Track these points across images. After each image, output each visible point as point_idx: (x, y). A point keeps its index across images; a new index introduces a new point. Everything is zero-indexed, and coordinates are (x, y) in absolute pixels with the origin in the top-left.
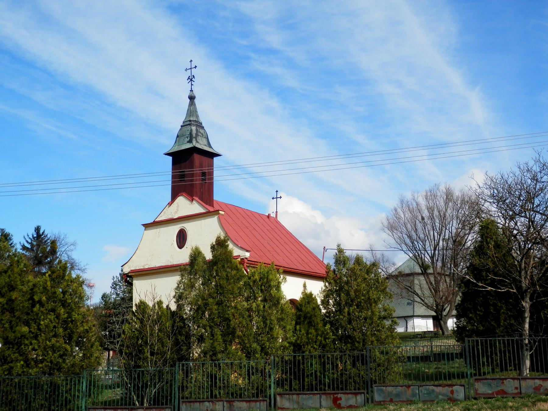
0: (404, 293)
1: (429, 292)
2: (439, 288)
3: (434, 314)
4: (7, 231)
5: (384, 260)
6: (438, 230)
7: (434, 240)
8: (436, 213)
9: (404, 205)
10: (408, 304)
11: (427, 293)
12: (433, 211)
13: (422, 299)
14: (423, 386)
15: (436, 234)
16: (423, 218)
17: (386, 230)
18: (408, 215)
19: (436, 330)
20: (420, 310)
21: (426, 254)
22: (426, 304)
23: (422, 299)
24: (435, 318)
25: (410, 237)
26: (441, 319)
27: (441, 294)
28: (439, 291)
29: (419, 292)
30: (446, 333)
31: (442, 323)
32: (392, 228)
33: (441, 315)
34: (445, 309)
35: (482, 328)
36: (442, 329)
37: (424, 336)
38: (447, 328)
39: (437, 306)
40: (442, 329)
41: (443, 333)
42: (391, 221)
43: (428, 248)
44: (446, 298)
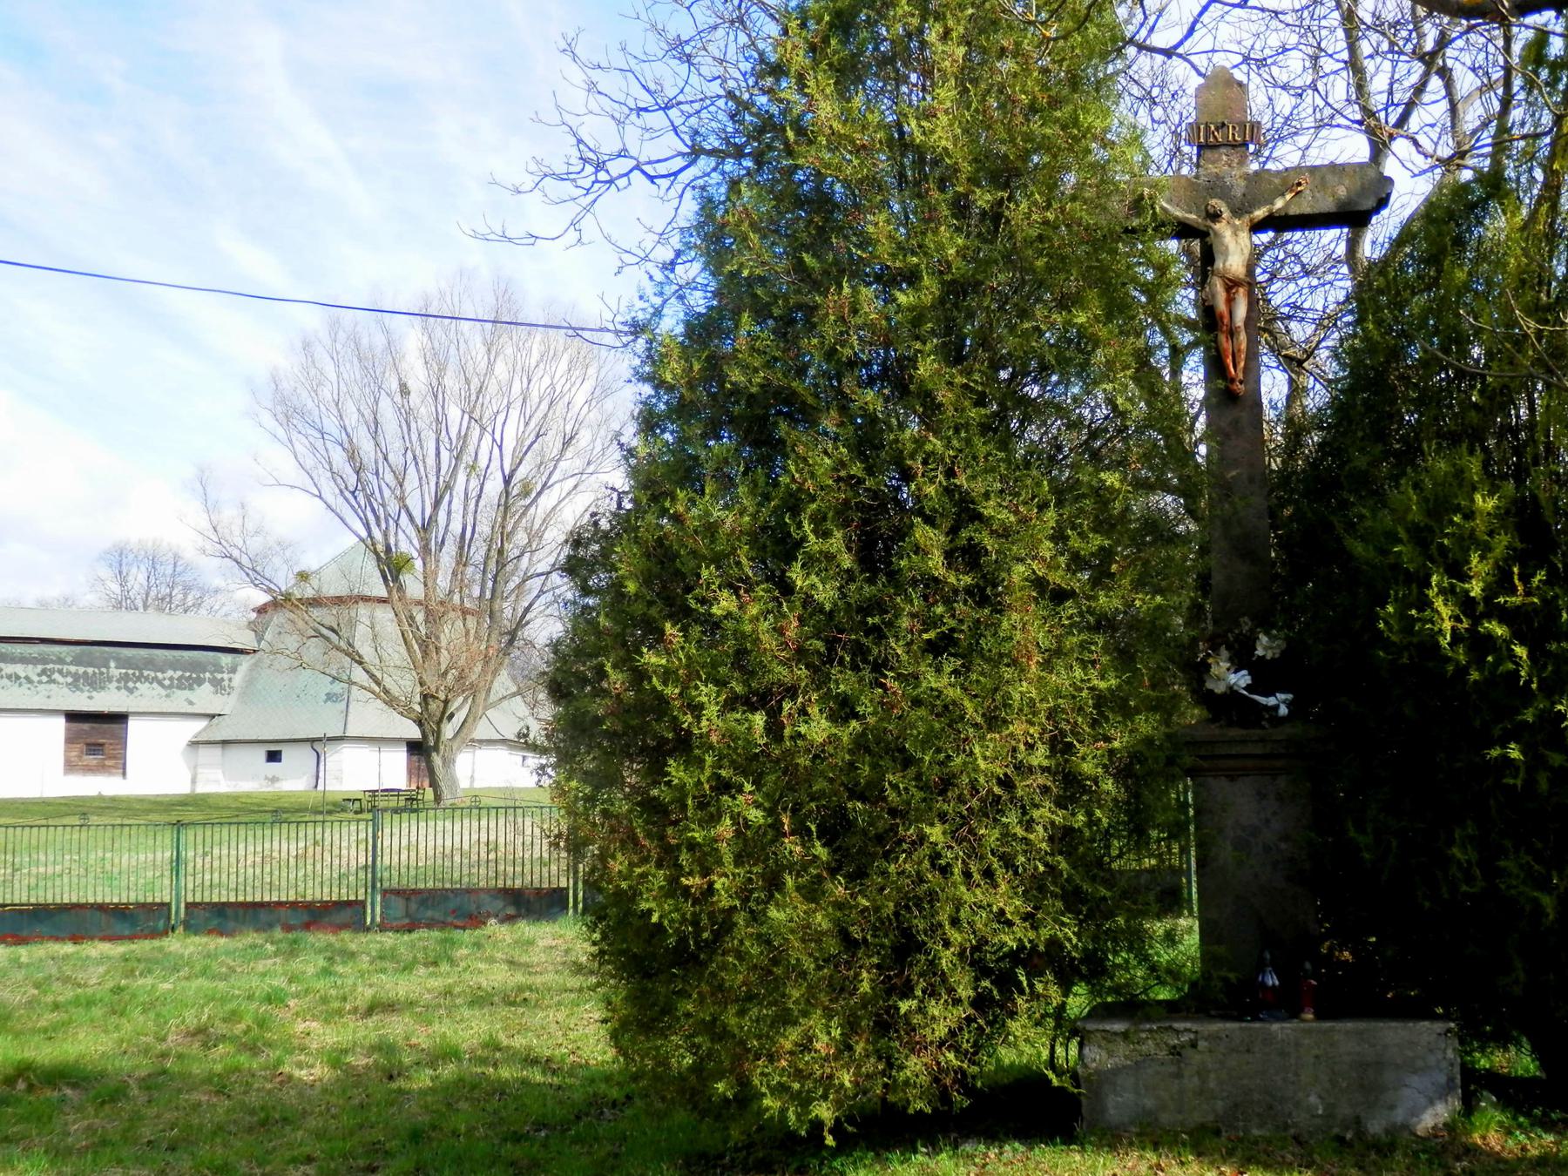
0: (314, 649)
1: (403, 649)
2: (438, 638)
3: (415, 733)
4: (185, 742)
5: (250, 526)
6: (454, 436)
7: (439, 470)
8: (452, 382)
9: (342, 336)
10: (330, 697)
11: (396, 653)
12: (442, 369)
13: (372, 676)
14: (531, 605)
15: (445, 455)
16: (404, 390)
17: (267, 419)
18: (352, 371)
19: (414, 787)
20: (370, 716)
21: (404, 519)
22: (386, 692)
23: (372, 676)
24: (417, 749)
25: (352, 455)
26: (436, 748)
27: (445, 658)
28: (438, 649)
29: (366, 651)
30: (447, 799)
31: (437, 760)
32: (289, 414)
33: (438, 733)
34: (452, 716)
35: (818, 728)
36: (434, 784)
37: (370, 807)
38: (454, 782)
39: (426, 698)
40: (434, 784)
41: (438, 798)
42: (286, 386)
43: (414, 503)
44: (461, 677)
